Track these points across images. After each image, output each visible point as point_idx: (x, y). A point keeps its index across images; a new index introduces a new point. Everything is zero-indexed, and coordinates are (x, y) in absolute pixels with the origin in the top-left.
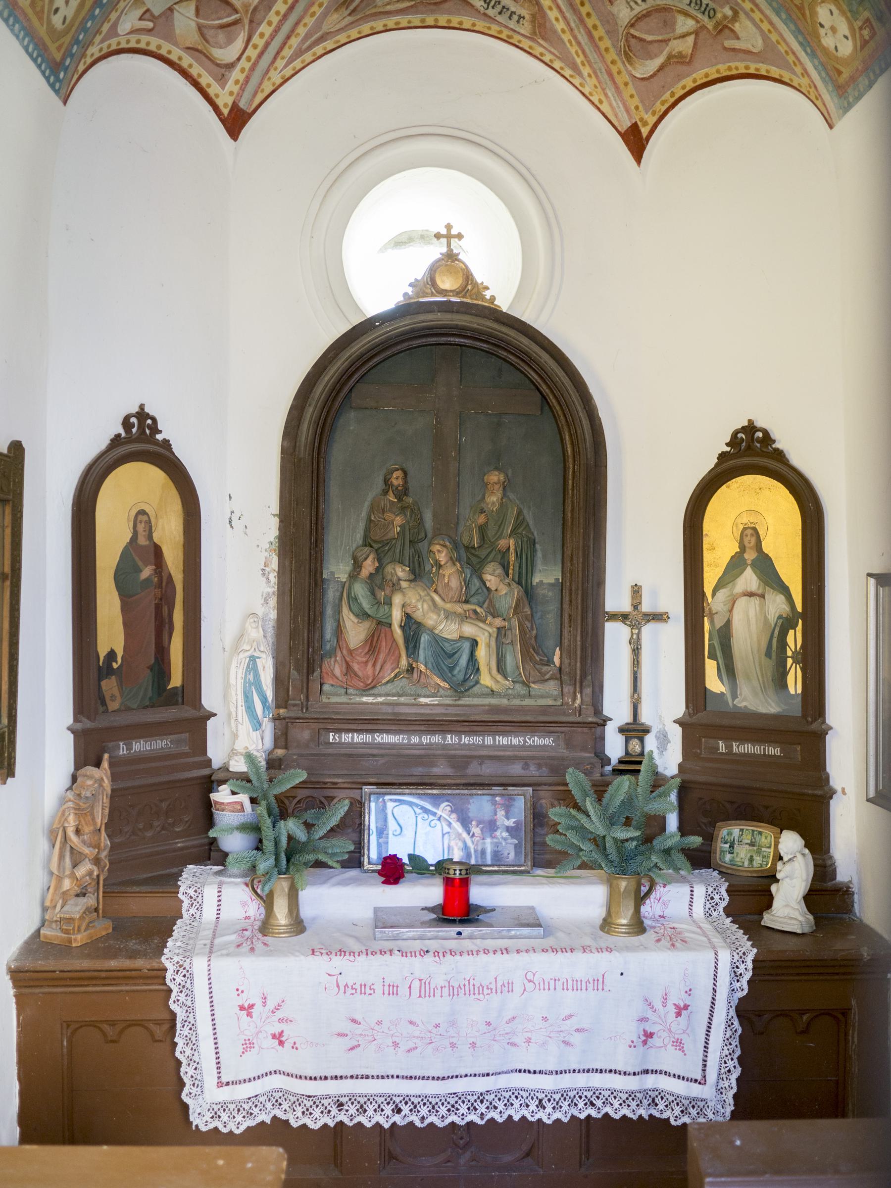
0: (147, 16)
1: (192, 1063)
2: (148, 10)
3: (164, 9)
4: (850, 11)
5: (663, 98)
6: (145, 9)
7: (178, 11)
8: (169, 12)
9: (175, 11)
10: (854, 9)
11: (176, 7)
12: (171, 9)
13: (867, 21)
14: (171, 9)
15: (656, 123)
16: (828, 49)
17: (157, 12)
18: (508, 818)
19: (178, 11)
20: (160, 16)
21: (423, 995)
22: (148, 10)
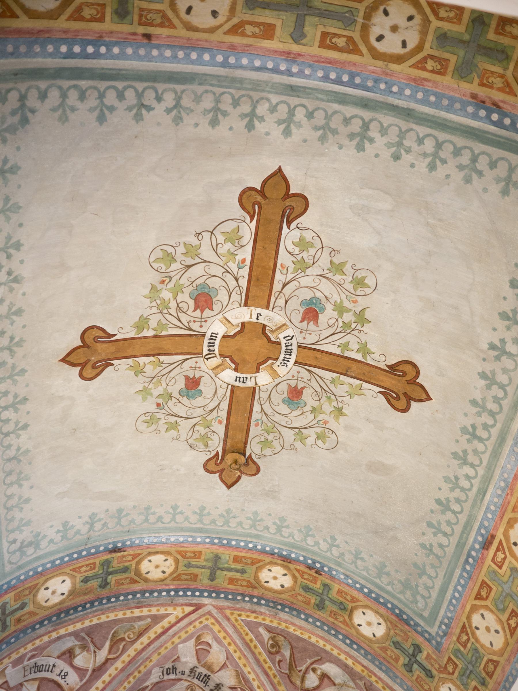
0: (5, 686)
1: (296, 378)
2: (6, 682)
3: (17, 683)
4: (462, 685)
5: (233, 620)
6: (4, 680)
7: (26, 687)
8: (20, 686)
9: (24, 687)
10: (465, 683)
11: (25, 683)
12: (21, 685)
13: (500, 567)
14: (21, 685)
15: (193, 613)
16: (485, 646)
17: (12, 684)
18: (343, 676)
19: (26, 687)
20: (13, 688)
21: (214, 355)
22: (6, 682)
